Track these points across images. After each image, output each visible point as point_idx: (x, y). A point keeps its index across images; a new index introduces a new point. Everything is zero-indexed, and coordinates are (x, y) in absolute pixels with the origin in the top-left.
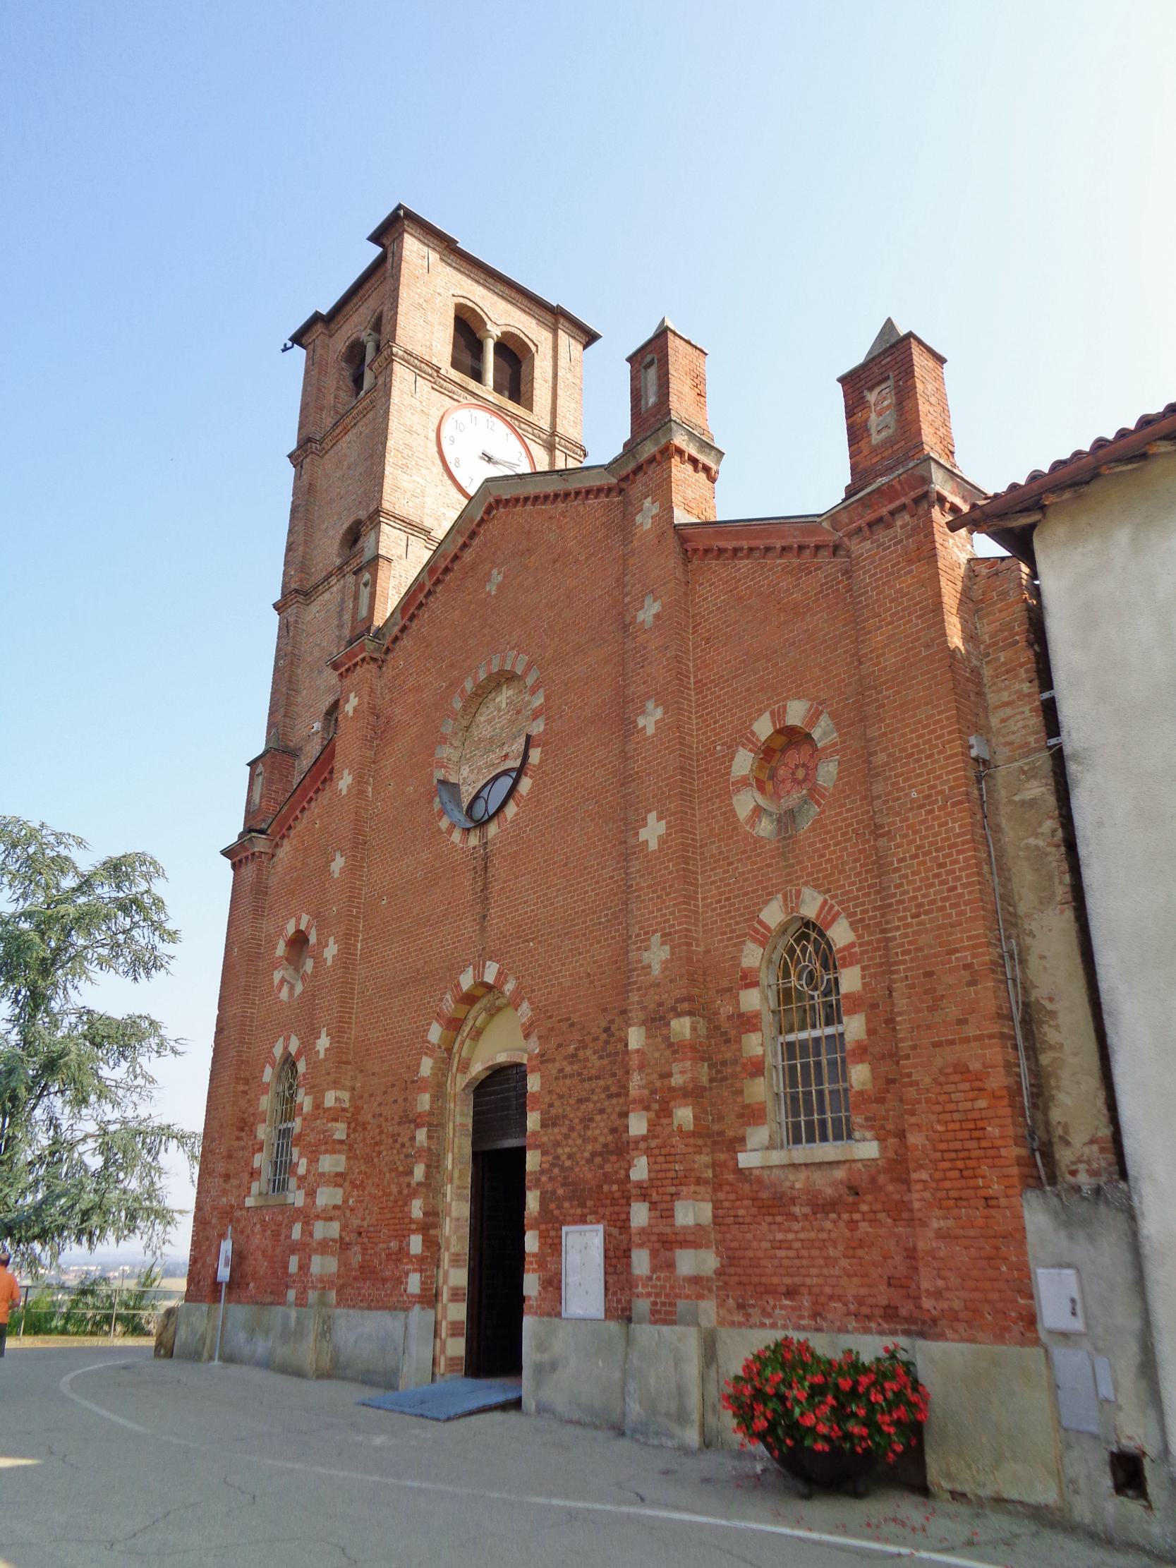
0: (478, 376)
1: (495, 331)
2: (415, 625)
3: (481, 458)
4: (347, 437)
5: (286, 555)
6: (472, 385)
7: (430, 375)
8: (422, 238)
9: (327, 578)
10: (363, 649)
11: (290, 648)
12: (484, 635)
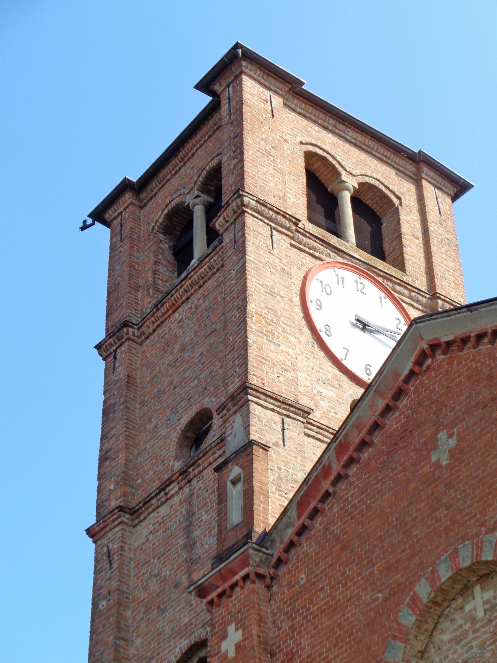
0: (337, 232)
1: (352, 183)
2: (318, 523)
3: (355, 325)
4: (176, 315)
5: (100, 466)
6: (334, 240)
7: (288, 229)
8: (262, 81)
9: (162, 488)
10: (245, 563)
11: (114, 584)
12: (438, 520)
